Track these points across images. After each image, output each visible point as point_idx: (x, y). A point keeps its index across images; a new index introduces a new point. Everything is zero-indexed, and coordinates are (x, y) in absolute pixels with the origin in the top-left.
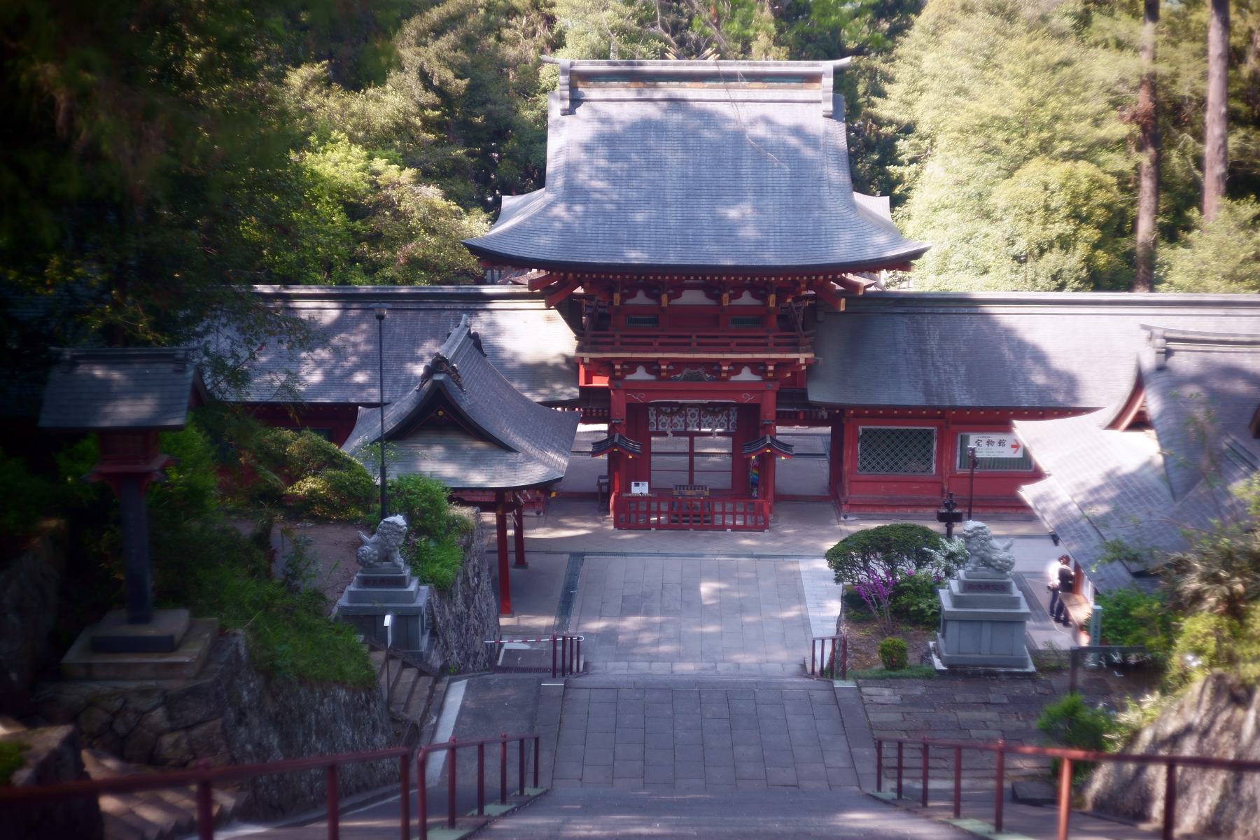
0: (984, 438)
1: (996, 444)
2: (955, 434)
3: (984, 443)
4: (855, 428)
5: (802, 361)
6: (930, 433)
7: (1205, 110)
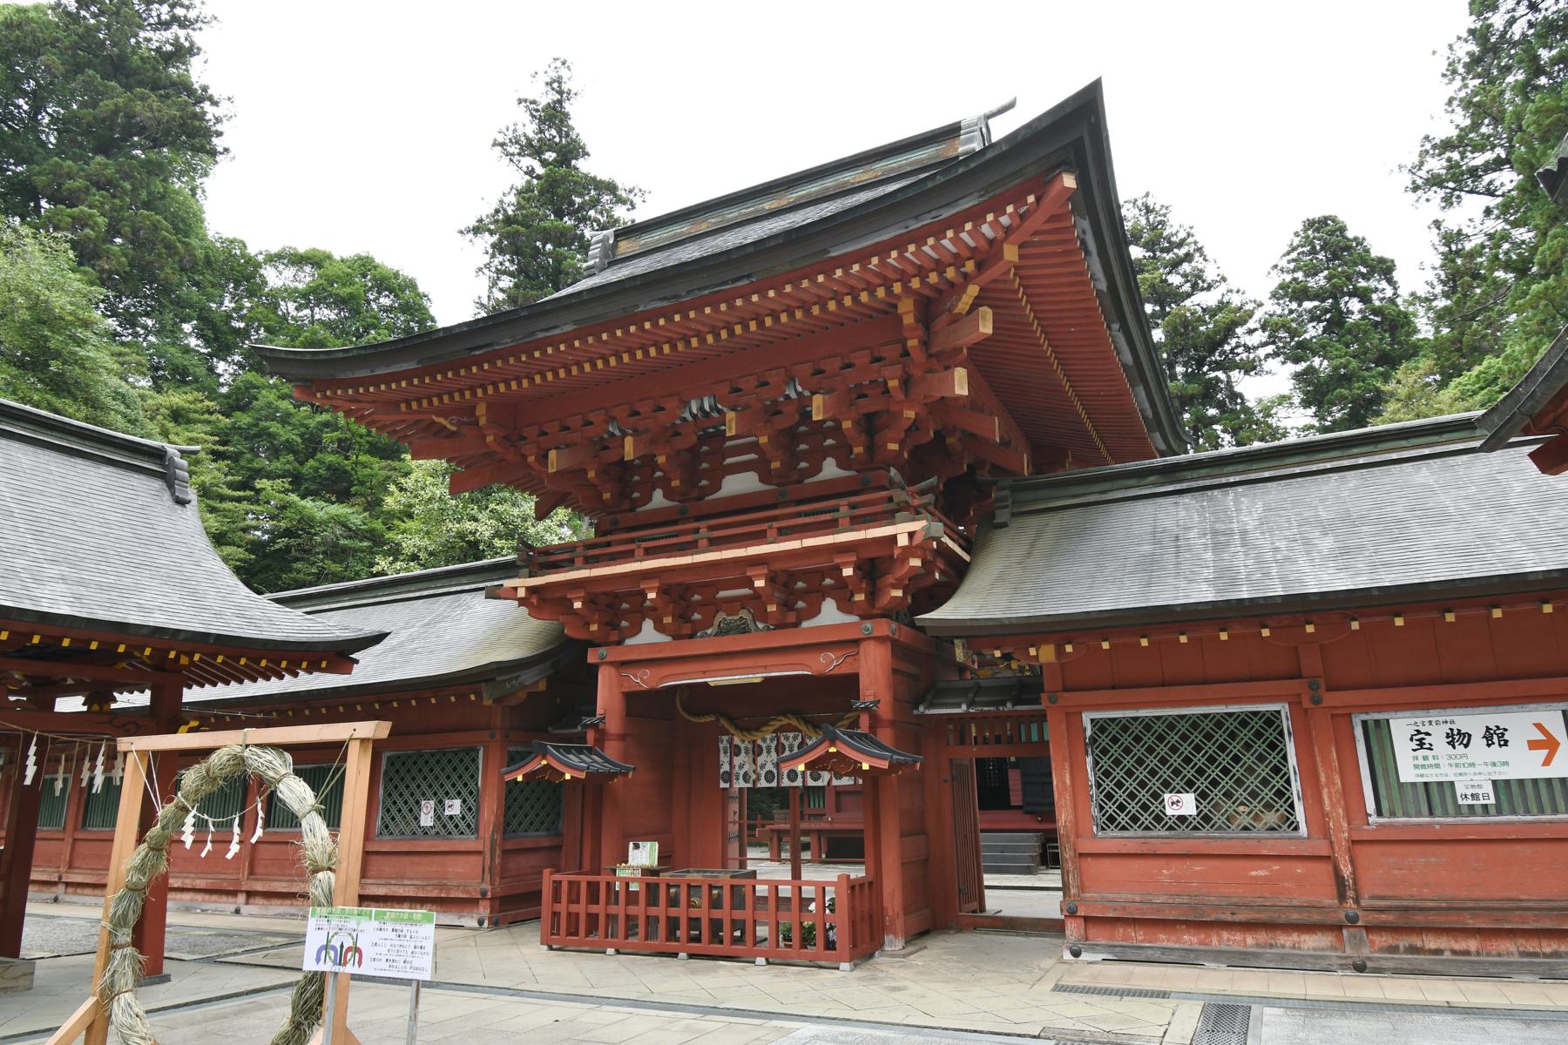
0: (1437, 725)
1: (1478, 741)
2: (1342, 719)
3: (1438, 738)
4: (1073, 717)
5: (903, 541)
6: (1272, 720)
7: (670, 586)
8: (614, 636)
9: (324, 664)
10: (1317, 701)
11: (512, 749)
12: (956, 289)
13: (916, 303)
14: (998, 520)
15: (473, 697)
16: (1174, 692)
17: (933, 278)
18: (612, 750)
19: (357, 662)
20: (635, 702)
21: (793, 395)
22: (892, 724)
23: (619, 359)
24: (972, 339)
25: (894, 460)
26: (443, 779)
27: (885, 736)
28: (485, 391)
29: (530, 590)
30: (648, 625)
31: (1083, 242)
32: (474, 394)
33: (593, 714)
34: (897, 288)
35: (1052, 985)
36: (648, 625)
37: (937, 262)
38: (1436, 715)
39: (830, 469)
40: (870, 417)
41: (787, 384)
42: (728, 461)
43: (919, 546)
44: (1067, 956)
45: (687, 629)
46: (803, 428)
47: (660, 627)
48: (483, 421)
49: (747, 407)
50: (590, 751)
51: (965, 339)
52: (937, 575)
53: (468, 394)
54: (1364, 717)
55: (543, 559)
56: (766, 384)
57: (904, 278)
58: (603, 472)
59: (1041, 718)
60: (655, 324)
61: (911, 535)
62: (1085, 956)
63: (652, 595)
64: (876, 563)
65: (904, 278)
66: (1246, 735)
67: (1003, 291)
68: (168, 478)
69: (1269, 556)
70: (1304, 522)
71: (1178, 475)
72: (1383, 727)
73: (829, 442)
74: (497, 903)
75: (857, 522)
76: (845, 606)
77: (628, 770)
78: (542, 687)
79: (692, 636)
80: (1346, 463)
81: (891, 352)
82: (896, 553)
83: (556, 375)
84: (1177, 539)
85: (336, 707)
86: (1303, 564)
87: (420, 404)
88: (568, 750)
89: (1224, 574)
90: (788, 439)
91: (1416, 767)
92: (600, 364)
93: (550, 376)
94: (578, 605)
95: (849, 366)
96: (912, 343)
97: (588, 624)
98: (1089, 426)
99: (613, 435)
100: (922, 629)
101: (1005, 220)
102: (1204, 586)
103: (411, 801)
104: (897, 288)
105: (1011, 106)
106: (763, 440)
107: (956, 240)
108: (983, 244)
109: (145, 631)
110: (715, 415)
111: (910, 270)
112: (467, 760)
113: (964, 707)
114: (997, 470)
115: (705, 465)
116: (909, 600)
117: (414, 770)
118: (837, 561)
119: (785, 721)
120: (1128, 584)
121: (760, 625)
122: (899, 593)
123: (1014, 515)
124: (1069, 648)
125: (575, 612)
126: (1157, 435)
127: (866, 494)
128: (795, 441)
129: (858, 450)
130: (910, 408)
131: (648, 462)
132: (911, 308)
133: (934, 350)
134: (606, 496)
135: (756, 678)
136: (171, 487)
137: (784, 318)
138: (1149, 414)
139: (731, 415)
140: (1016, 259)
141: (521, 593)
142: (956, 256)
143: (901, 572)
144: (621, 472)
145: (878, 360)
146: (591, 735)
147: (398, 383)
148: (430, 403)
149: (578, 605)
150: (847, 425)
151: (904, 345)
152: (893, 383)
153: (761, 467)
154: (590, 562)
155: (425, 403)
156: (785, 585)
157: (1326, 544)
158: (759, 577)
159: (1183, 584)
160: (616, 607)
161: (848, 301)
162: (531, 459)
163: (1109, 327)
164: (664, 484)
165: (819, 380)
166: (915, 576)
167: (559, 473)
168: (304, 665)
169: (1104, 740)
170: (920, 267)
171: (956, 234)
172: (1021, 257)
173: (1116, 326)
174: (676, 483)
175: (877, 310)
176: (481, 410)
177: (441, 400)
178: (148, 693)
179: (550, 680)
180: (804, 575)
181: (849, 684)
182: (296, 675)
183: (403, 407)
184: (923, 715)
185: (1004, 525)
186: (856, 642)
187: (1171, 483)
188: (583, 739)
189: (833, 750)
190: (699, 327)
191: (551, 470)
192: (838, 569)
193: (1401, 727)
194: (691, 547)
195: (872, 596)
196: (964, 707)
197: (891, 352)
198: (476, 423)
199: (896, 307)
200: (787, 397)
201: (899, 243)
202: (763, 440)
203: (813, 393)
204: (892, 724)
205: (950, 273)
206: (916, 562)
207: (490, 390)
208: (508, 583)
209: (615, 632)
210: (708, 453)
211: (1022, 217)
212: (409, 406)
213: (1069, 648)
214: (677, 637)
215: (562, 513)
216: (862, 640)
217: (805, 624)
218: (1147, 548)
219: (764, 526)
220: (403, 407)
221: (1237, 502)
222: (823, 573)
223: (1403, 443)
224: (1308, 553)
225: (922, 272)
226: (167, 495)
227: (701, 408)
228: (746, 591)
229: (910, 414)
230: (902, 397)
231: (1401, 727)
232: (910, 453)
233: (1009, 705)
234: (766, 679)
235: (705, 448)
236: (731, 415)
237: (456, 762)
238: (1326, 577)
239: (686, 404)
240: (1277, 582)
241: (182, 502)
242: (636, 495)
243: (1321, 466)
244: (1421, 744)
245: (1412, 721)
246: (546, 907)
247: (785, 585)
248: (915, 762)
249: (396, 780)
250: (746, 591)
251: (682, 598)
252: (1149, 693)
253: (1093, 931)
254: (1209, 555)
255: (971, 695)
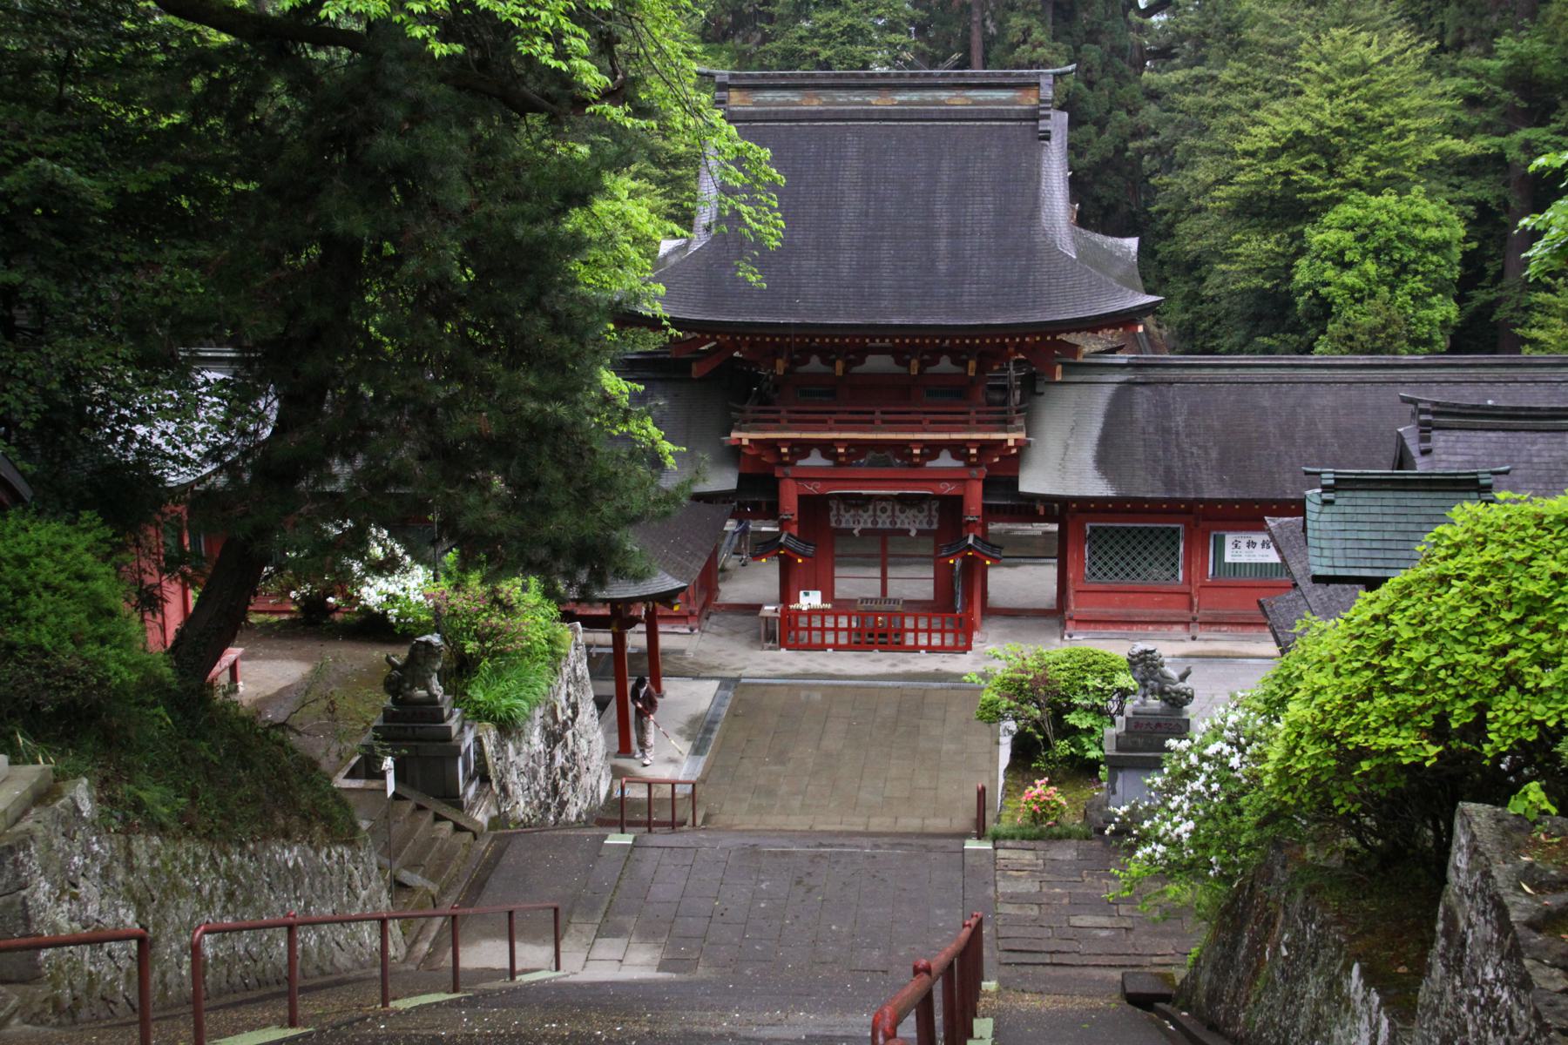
0: (1244, 538)
1: (1259, 546)
3: (1243, 544)
6: (1175, 531)
38: (1243, 534)
66: (1162, 538)
169: (1095, 537)
193: (1229, 538)
231: (1229, 538)
253: (1000, 843)
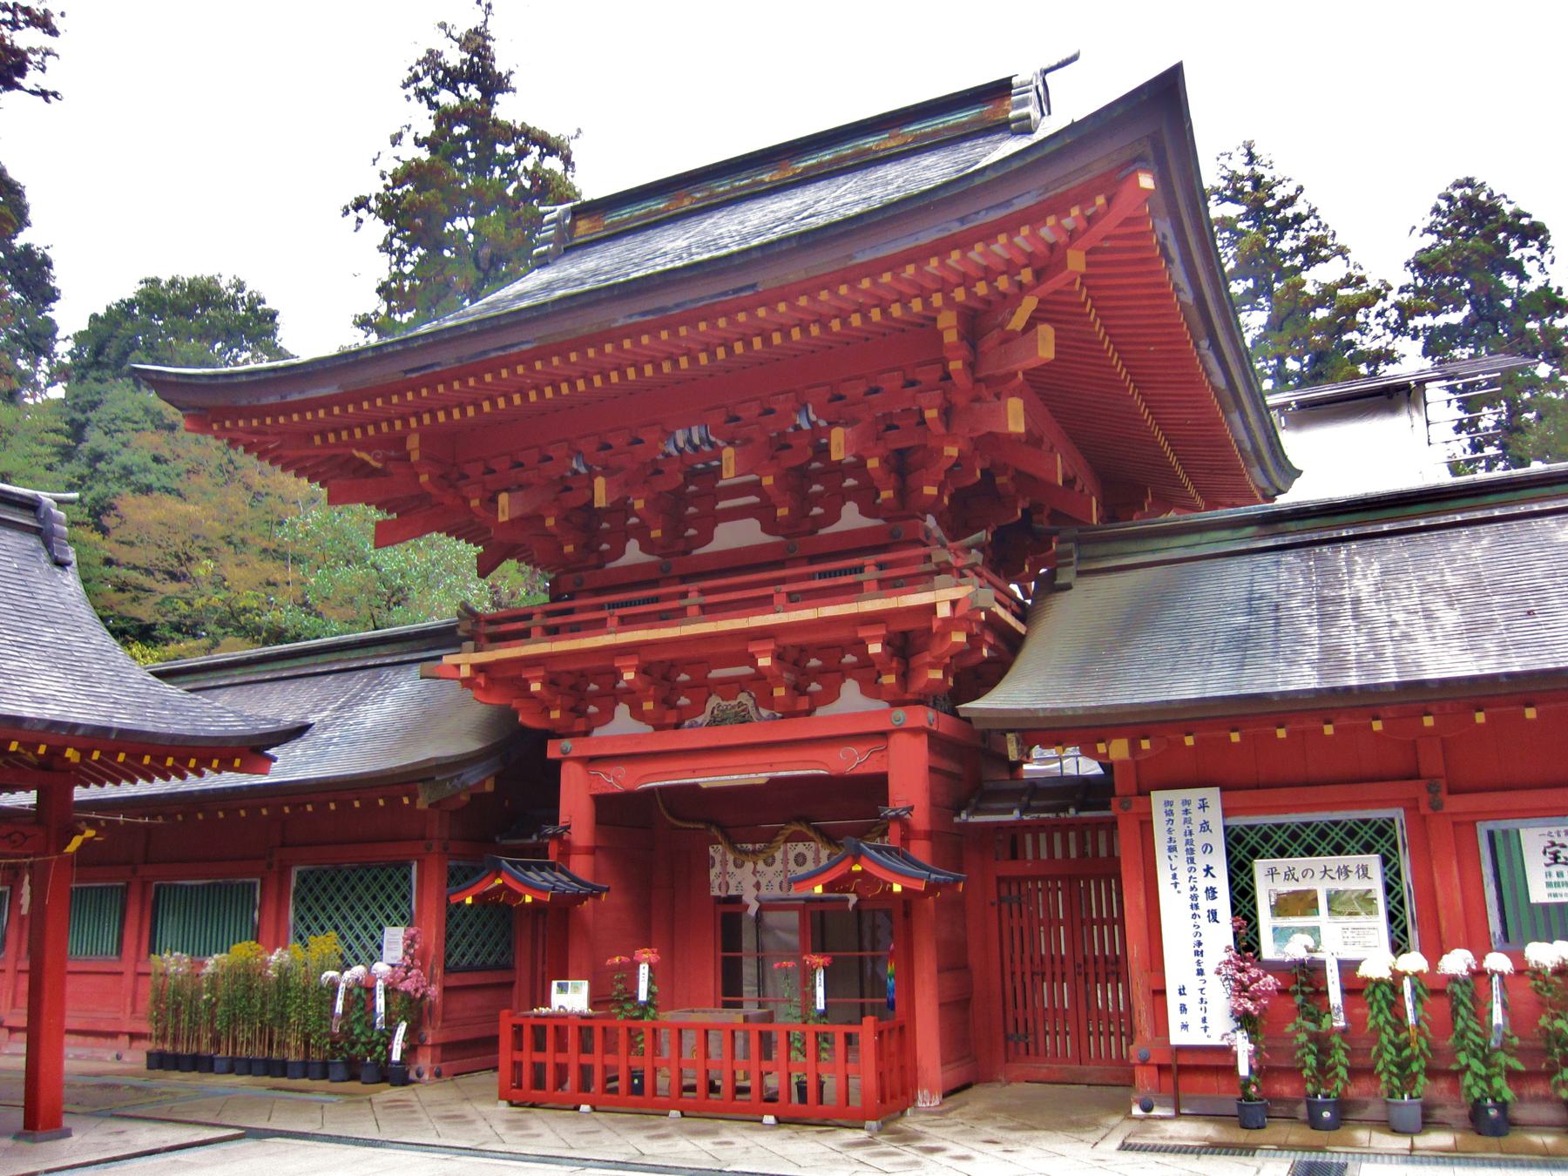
7: (651, 663)
8: (580, 725)
9: (237, 763)
10: (1436, 807)
11: (451, 863)
12: (1009, 301)
13: (959, 315)
14: (1060, 581)
15: (406, 801)
16: (1309, 794)
17: (981, 289)
18: (581, 865)
19: (274, 759)
20: (608, 807)
21: (806, 426)
22: (929, 835)
23: (589, 382)
24: (1031, 363)
25: (932, 506)
26: (367, 898)
27: (920, 850)
28: (420, 421)
29: (478, 668)
30: (622, 710)
31: (1164, 249)
32: (406, 423)
33: (554, 820)
34: (937, 299)
35: (1118, 1143)
36: (622, 710)
37: (986, 269)
39: (851, 518)
40: (901, 453)
41: (797, 411)
42: (722, 505)
43: (964, 618)
44: (1137, 1111)
45: (672, 717)
46: (816, 465)
47: (637, 713)
48: (415, 456)
49: (748, 441)
50: (553, 867)
51: (1021, 363)
52: (985, 652)
53: (398, 425)
54: (1490, 825)
55: (492, 629)
56: (771, 411)
57: (945, 287)
58: (563, 520)
59: (1111, 825)
60: (637, 343)
61: (954, 603)
62: (1156, 1112)
63: (629, 676)
64: (909, 638)
65: (945, 287)
67: (1071, 304)
68: (45, 535)
69: (1383, 632)
70: (1428, 589)
71: (1281, 527)
72: (1512, 838)
73: (850, 482)
74: (438, 1051)
75: (888, 586)
76: (871, 688)
77: (601, 890)
78: (489, 786)
79: (678, 726)
80: (1479, 515)
81: (928, 375)
82: (935, 625)
83: (509, 401)
84: (1277, 608)
85: (237, 810)
86: (1423, 642)
87: (338, 436)
88: (527, 867)
89: (1331, 656)
90: (795, 481)
91: (1549, 885)
92: (565, 388)
93: (501, 403)
94: (536, 687)
95: (876, 391)
96: (955, 365)
97: (547, 710)
98: (1173, 459)
99: (576, 472)
100: (968, 720)
101: (1068, 223)
102: (1306, 669)
103: (372, 926)
104: (937, 299)
105: (1074, 58)
106: (768, 481)
107: (1010, 244)
108: (1042, 249)
109: (40, 727)
110: (707, 448)
111: (953, 279)
112: (398, 877)
113: (1016, 813)
114: (1057, 517)
115: (692, 510)
116: (951, 682)
117: (332, 890)
118: (862, 633)
119: (795, 827)
120: (1217, 665)
121: (764, 713)
122: (937, 675)
123: (1080, 574)
124: (1145, 744)
125: (533, 696)
126: (1256, 471)
127: (893, 549)
128: (803, 485)
129: (886, 494)
130: (953, 443)
131: (620, 508)
132: (954, 322)
133: (982, 374)
134: (569, 549)
135: (761, 778)
136: (48, 544)
137: (796, 334)
138: (1248, 446)
139: (729, 453)
140: (1082, 268)
141: (465, 672)
142: (1009, 262)
143: (939, 649)
144: (585, 519)
145: (912, 383)
146: (553, 848)
147: (315, 412)
148: (351, 434)
149: (536, 687)
150: (873, 463)
151: (945, 366)
152: (931, 414)
153: (763, 513)
154: (552, 632)
155: (344, 435)
156: (795, 663)
157: (1450, 618)
158: (763, 653)
159: (1282, 666)
160: (584, 689)
161: (876, 315)
162: (475, 503)
163: (1197, 345)
164: (641, 532)
165: (838, 410)
166: (959, 654)
167: (512, 521)
168: (215, 763)
170: (965, 275)
171: (1010, 238)
172: (1088, 264)
173: (1204, 344)
174: (656, 533)
175: (912, 324)
176: (413, 442)
177: (365, 432)
178: (34, 793)
179: (498, 778)
180: (820, 650)
181: (874, 787)
182: (201, 774)
183: (317, 440)
184: (966, 824)
185: (1068, 587)
186: (884, 735)
187: (1272, 535)
188: (541, 851)
189: (857, 868)
190: (691, 345)
191: (503, 518)
192: (862, 644)
193: (1533, 839)
194: (678, 615)
195: (905, 677)
196: (1016, 813)
197: (928, 375)
198: (406, 457)
199: (935, 320)
200: (798, 428)
201: (940, 248)
202: (768, 481)
203: (832, 424)
204: (929, 835)
205: (1003, 283)
206: (959, 637)
207: (427, 419)
208: (449, 660)
209: (580, 723)
210: (695, 495)
211: (1090, 220)
212: (325, 439)
213: (1145, 744)
214: (659, 727)
215: (510, 566)
216: (892, 732)
217: (821, 712)
218: (1241, 620)
219: (770, 590)
220: (317, 440)
221: (1350, 562)
222: (843, 648)
223: (1546, 491)
224: (1430, 628)
225: (967, 281)
226: (44, 556)
227: (689, 441)
228: (746, 670)
229: (952, 451)
230: (943, 430)
231: (1533, 839)
232: (951, 498)
233: (1072, 811)
234: (772, 781)
235: (692, 488)
236: (729, 453)
237: (383, 878)
238: (1448, 659)
239: (669, 435)
240: (1391, 665)
241: (62, 565)
242: (605, 547)
243: (1450, 518)
244: (1556, 858)
245: (1546, 830)
246: (505, 1056)
247: (795, 663)
248: (957, 881)
249: (310, 900)
250: (746, 670)
251: (665, 678)
252: (1284, 795)
254: (1313, 630)
255: (1025, 799)
